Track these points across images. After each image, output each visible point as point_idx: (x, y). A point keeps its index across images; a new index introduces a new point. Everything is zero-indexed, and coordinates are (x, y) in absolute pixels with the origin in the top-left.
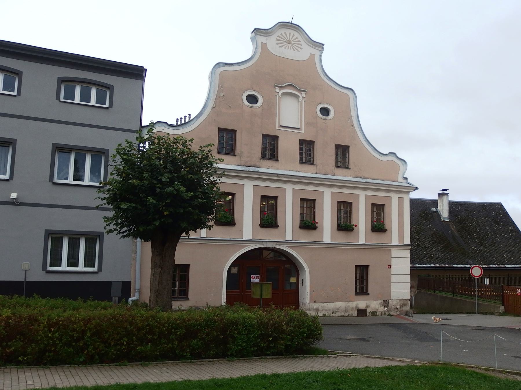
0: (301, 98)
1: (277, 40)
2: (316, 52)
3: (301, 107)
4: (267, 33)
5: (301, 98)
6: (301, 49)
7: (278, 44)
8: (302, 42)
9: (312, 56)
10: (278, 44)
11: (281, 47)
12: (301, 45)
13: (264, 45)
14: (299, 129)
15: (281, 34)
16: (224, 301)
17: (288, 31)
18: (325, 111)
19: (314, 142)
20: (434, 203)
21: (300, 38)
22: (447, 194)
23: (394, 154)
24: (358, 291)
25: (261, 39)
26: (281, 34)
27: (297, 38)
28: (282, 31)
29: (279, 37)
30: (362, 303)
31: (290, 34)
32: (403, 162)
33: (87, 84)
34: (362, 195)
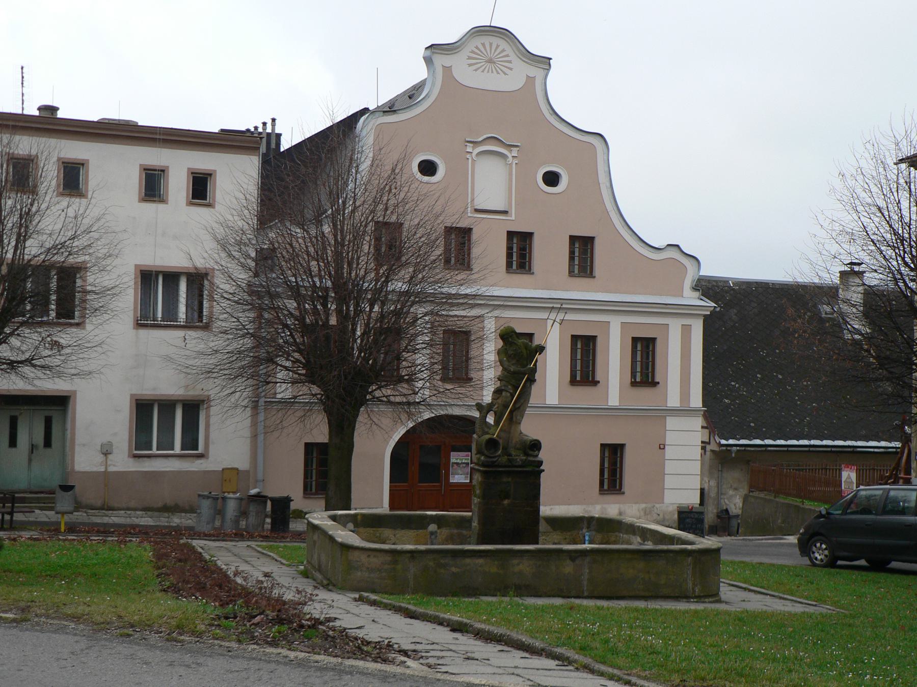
0: (510, 159)
1: (470, 58)
2: (535, 71)
4: (456, 49)
5: (510, 159)
6: (511, 69)
7: (470, 65)
8: (513, 57)
9: (530, 80)
10: (470, 65)
11: (476, 70)
12: (510, 62)
13: (447, 70)
14: (505, 212)
15: (477, 48)
17: (487, 40)
19: (531, 235)
20: (829, 293)
21: (509, 50)
22: (860, 274)
23: (678, 246)
24: (606, 487)
25: (440, 60)
26: (477, 48)
27: (503, 50)
28: (478, 41)
29: (473, 52)
30: (610, 508)
31: (491, 44)
32: (695, 263)
34: (615, 324)
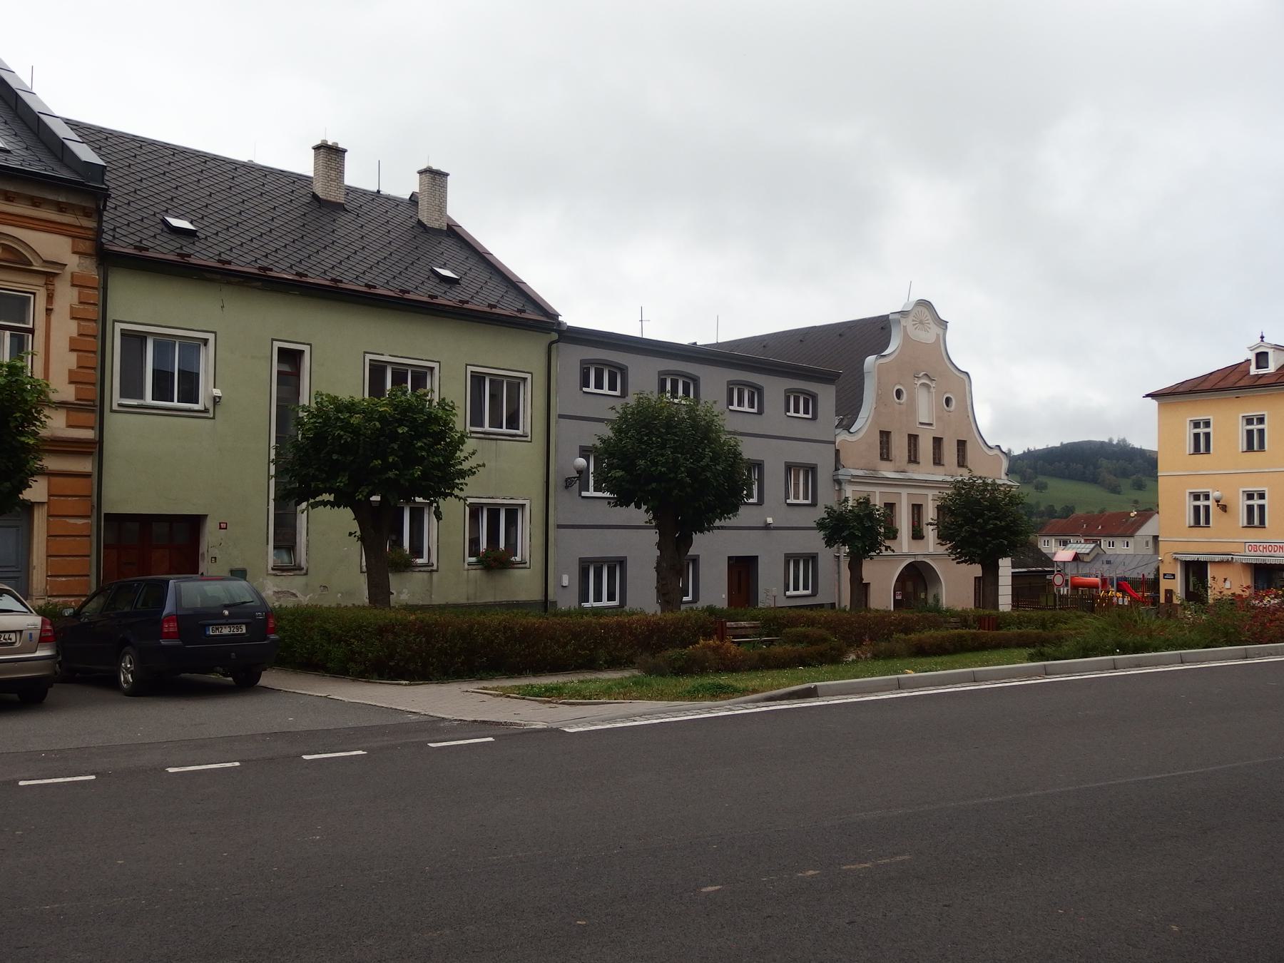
3: (932, 400)
16: (892, 609)
17: (925, 310)
18: (948, 401)
33: (600, 366)
